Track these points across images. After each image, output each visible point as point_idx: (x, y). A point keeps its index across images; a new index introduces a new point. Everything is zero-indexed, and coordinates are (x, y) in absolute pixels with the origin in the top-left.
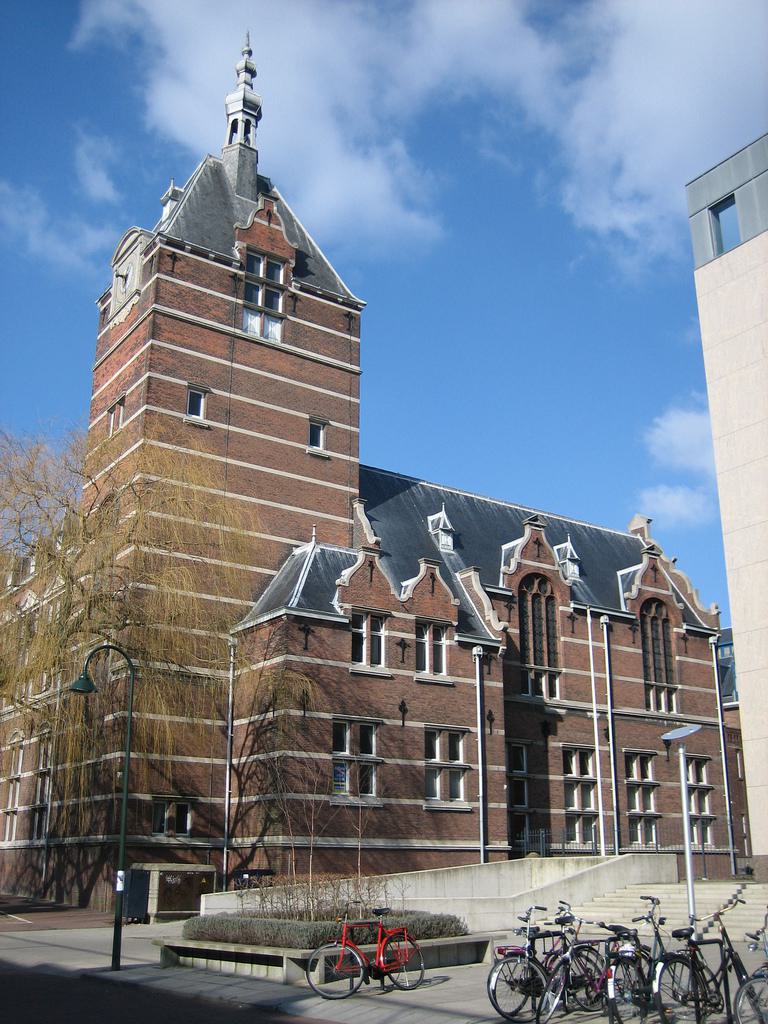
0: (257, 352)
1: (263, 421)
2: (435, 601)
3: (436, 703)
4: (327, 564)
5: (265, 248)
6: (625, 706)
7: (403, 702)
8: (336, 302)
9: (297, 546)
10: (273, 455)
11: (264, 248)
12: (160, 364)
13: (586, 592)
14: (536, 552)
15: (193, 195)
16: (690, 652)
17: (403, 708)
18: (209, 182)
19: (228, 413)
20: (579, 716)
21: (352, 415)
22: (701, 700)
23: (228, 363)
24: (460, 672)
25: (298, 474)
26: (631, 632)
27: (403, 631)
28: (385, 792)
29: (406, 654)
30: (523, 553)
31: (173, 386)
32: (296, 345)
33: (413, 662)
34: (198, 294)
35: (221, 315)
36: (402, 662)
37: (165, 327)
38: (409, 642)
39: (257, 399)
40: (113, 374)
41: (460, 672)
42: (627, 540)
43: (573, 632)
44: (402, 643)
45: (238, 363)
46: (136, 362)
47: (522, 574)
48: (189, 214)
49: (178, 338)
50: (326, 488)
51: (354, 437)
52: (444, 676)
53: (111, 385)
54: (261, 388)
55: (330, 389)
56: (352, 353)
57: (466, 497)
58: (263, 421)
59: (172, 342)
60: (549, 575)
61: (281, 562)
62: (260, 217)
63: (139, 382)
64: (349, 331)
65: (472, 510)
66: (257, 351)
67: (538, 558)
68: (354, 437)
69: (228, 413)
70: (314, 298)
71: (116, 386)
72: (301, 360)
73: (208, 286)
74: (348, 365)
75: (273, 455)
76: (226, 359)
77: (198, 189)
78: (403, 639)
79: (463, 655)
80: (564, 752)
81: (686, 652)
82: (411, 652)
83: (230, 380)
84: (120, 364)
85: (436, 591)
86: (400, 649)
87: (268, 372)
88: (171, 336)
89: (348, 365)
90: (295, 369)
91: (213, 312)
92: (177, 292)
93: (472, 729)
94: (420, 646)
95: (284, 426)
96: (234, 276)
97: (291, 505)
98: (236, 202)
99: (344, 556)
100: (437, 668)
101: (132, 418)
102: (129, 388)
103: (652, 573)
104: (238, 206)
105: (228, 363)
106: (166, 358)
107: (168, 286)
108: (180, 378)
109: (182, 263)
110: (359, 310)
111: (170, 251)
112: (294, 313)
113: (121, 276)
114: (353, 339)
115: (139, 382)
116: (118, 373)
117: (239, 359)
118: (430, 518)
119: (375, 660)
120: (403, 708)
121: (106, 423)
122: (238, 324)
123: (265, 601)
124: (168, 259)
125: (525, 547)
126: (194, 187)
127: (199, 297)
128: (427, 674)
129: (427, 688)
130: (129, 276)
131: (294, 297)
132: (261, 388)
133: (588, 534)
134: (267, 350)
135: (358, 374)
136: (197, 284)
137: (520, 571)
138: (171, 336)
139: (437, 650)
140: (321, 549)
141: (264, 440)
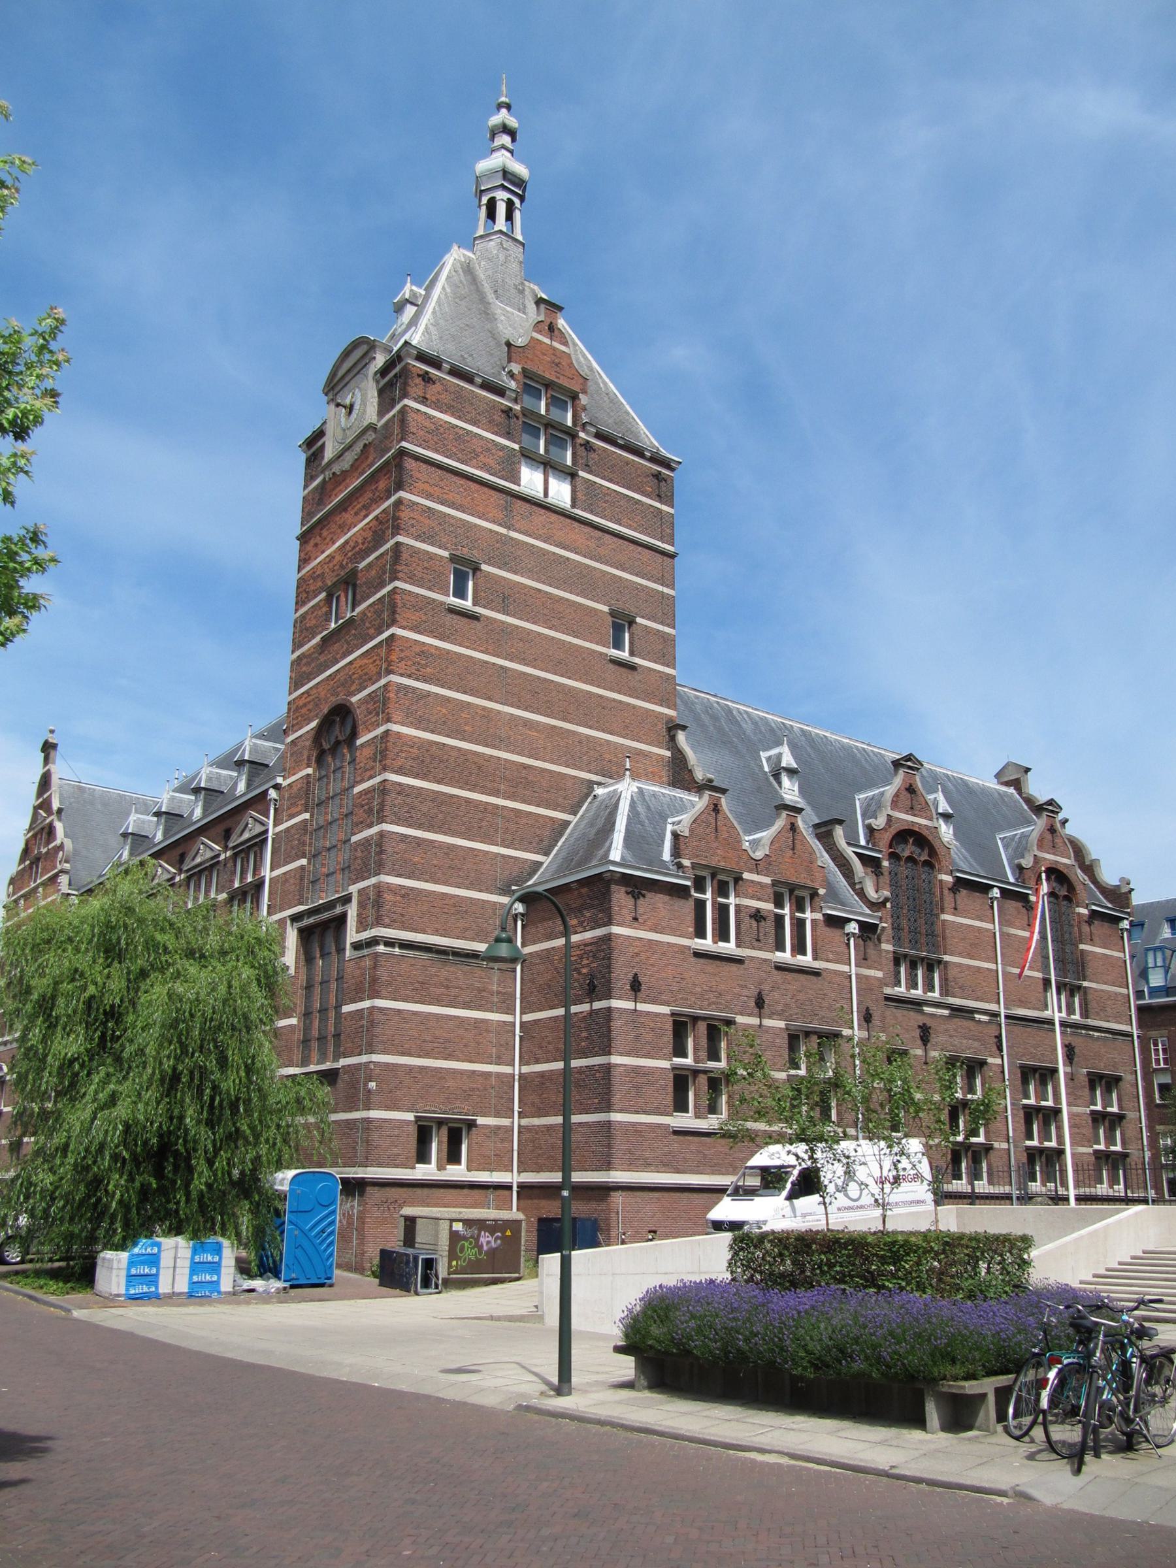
0: (541, 518)
1: (551, 612)
2: (798, 861)
3: (801, 996)
4: (648, 808)
5: (549, 375)
6: (1019, 1006)
7: (760, 993)
8: (642, 455)
9: (599, 784)
10: (568, 659)
11: (547, 375)
12: (413, 526)
13: (965, 858)
14: (908, 803)
15: (443, 297)
16: (1096, 939)
17: (760, 1003)
18: (461, 282)
19: (506, 598)
20: (964, 1018)
21: (665, 610)
22: (1109, 1002)
23: (503, 530)
24: (831, 956)
25: (598, 686)
26: (1024, 910)
27: (759, 899)
28: (734, 1114)
29: (761, 930)
30: (895, 803)
31: (431, 557)
32: (591, 512)
33: (771, 939)
34: (462, 432)
35: (492, 463)
36: (758, 943)
37: (419, 475)
38: (765, 914)
39: (543, 583)
40: (334, 543)
41: (831, 956)
42: (999, 794)
43: (955, 909)
44: (757, 916)
45: (516, 531)
46: (375, 522)
47: (893, 831)
48: (441, 322)
49: (437, 491)
50: (634, 707)
51: (668, 641)
52: (806, 960)
53: (331, 557)
54: (547, 567)
55: (637, 575)
56: (665, 526)
57: (802, 730)
58: (551, 612)
59: (429, 496)
60: (925, 833)
61: (579, 805)
62: (540, 332)
63: (382, 550)
64: (659, 498)
65: (812, 747)
66: (541, 516)
67: (911, 810)
68: (668, 641)
69: (506, 598)
70: (613, 449)
71: (338, 558)
72: (600, 534)
73: (474, 423)
74: (659, 543)
75: (568, 659)
76: (500, 525)
77: (448, 290)
78: (758, 910)
79: (834, 934)
80: (676, 1076)
81: (1091, 940)
82: (769, 926)
83: (507, 554)
84: (345, 528)
85: (798, 846)
86: (754, 923)
87: (557, 546)
88: (427, 487)
89: (659, 543)
90: (592, 544)
91: (481, 458)
92: (433, 427)
93: (846, 1032)
94: (779, 919)
95: (578, 622)
96: (508, 412)
97: (590, 727)
98: (499, 311)
99: (668, 799)
100: (799, 948)
101: (371, 600)
102: (364, 559)
103: (1049, 836)
104: (503, 318)
105: (503, 530)
106: (422, 519)
107: (420, 419)
108: (440, 547)
109: (437, 387)
110: (672, 469)
111: (421, 369)
112: (588, 468)
113: (345, 407)
114: (665, 508)
115: (382, 550)
116: (342, 541)
117: (517, 526)
118: (764, 755)
119: (722, 934)
120: (760, 1003)
121: (324, 609)
122: (515, 479)
123: (563, 854)
124: (418, 380)
125: (897, 795)
126: (443, 288)
127: (462, 437)
128: (786, 956)
129: (790, 976)
130: (357, 407)
131: (587, 446)
132: (547, 567)
133: (953, 785)
134: (554, 517)
135: (672, 556)
136: (459, 418)
137: (890, 826)
138: (427, 487)
139: (799, 925)
140: (638, 787)
141: (553, 638)
